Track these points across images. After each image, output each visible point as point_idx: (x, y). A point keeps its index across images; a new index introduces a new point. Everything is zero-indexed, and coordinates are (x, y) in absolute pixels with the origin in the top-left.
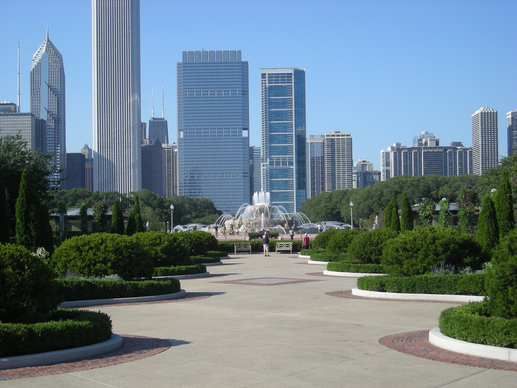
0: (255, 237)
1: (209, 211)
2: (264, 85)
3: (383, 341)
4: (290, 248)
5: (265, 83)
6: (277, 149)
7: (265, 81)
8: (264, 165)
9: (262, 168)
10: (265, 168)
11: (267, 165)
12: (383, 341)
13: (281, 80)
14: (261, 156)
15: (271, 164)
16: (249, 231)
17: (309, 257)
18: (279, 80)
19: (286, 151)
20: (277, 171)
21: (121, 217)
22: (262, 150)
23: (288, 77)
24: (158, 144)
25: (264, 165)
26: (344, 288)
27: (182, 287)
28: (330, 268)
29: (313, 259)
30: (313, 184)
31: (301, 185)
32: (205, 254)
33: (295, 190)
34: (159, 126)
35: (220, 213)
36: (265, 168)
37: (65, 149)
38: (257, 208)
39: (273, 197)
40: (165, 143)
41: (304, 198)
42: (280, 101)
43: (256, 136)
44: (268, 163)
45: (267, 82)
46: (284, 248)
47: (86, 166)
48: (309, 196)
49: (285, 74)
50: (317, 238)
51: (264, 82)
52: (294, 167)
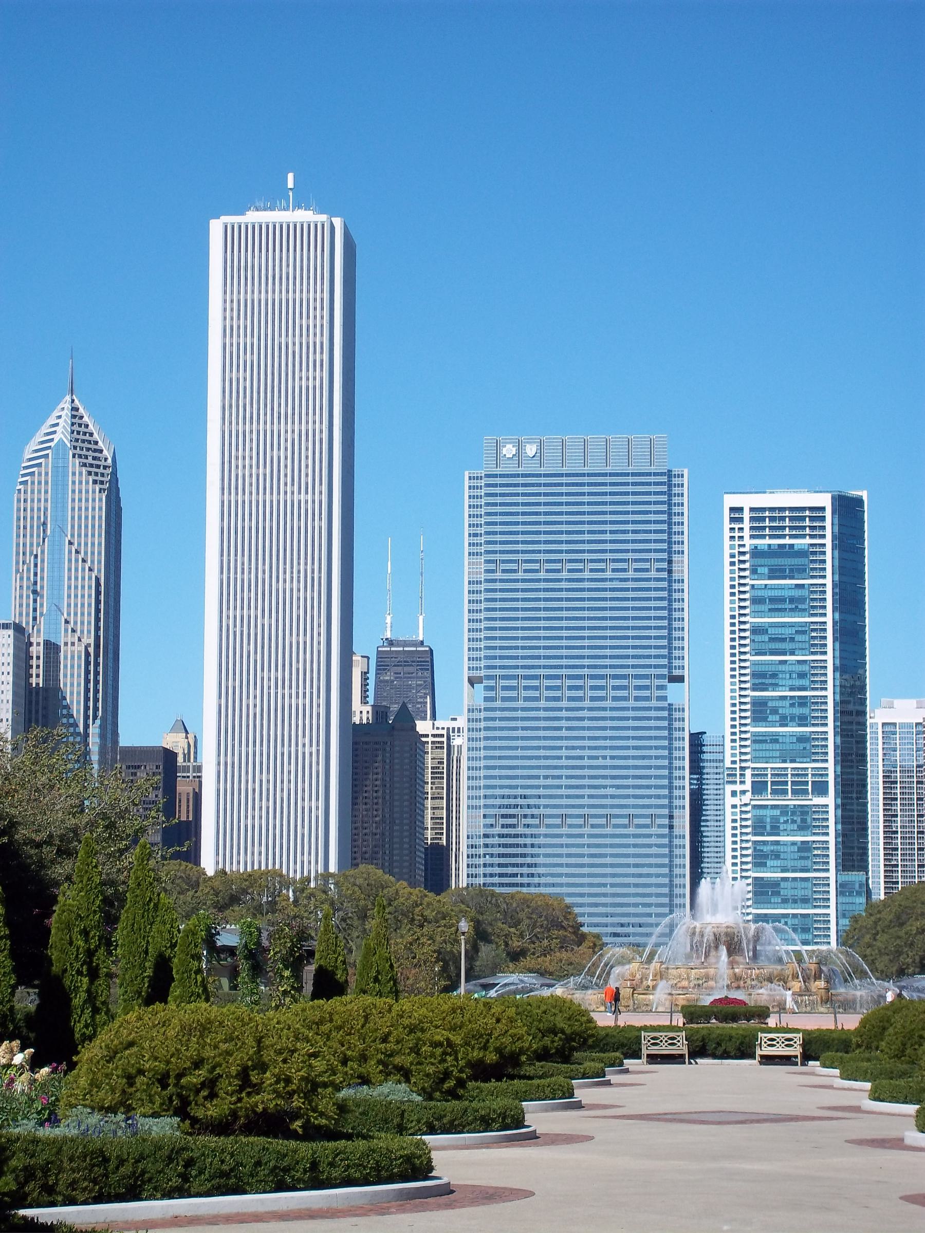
0: (700, 1016)
1: (557, 935)
2: (737, 543)
3: (901, 1198)
4: (797, 1051)
5: (741, 538)
6: (776, 741)
7: (741, 529)
8: (734, 794)
9: (729, 801)
10: (736, 801)
11: (743, 792)
12: (901, 1198)
13: (791, 528)
14: (728, 764)
15: (758, 787)
16: (681, 1001)
17: (837, 1072)
18: (784, 528)
19: (806, 747)
20: (777, 812)
21: (297, 951)
22: (728, 744)
23: (812, 519)
24: (406, 719)
25: (734, 794)
26: (893, 1134)
27: (529, 1119)
28: (876, 1096)
29: (845, 1076)
30: (890, 851)
31: (853, 855)
32: (572, 1051)
33: (832, 874)
34: (409, 668)
35: (597, 945)
36: (736, 801)
37: (115, 734)
38: (709, 931)
39: (763, 891)
40: (425, 719)
41: (862, 900)
42: (787, 593)
43: (713, 697)
44: (748, 786)
45: (746, 533)
46: (779, 1050)
47: (179, 788)
48: (880, 894)
49: (803, 509)
50: (863, 1023)
51: (737, 534)
52: (830, 800)
